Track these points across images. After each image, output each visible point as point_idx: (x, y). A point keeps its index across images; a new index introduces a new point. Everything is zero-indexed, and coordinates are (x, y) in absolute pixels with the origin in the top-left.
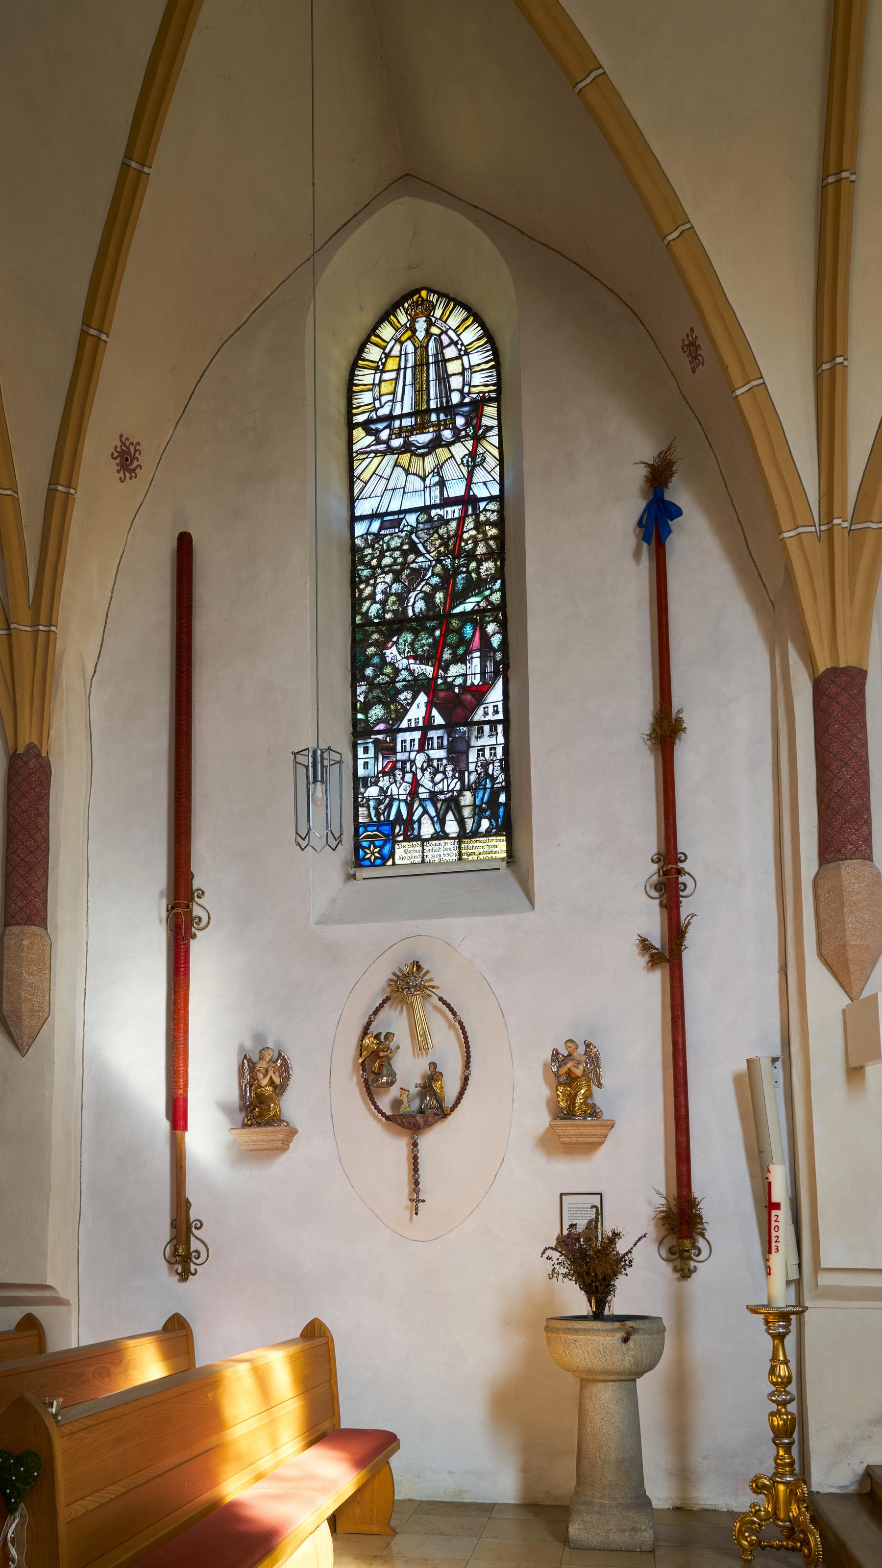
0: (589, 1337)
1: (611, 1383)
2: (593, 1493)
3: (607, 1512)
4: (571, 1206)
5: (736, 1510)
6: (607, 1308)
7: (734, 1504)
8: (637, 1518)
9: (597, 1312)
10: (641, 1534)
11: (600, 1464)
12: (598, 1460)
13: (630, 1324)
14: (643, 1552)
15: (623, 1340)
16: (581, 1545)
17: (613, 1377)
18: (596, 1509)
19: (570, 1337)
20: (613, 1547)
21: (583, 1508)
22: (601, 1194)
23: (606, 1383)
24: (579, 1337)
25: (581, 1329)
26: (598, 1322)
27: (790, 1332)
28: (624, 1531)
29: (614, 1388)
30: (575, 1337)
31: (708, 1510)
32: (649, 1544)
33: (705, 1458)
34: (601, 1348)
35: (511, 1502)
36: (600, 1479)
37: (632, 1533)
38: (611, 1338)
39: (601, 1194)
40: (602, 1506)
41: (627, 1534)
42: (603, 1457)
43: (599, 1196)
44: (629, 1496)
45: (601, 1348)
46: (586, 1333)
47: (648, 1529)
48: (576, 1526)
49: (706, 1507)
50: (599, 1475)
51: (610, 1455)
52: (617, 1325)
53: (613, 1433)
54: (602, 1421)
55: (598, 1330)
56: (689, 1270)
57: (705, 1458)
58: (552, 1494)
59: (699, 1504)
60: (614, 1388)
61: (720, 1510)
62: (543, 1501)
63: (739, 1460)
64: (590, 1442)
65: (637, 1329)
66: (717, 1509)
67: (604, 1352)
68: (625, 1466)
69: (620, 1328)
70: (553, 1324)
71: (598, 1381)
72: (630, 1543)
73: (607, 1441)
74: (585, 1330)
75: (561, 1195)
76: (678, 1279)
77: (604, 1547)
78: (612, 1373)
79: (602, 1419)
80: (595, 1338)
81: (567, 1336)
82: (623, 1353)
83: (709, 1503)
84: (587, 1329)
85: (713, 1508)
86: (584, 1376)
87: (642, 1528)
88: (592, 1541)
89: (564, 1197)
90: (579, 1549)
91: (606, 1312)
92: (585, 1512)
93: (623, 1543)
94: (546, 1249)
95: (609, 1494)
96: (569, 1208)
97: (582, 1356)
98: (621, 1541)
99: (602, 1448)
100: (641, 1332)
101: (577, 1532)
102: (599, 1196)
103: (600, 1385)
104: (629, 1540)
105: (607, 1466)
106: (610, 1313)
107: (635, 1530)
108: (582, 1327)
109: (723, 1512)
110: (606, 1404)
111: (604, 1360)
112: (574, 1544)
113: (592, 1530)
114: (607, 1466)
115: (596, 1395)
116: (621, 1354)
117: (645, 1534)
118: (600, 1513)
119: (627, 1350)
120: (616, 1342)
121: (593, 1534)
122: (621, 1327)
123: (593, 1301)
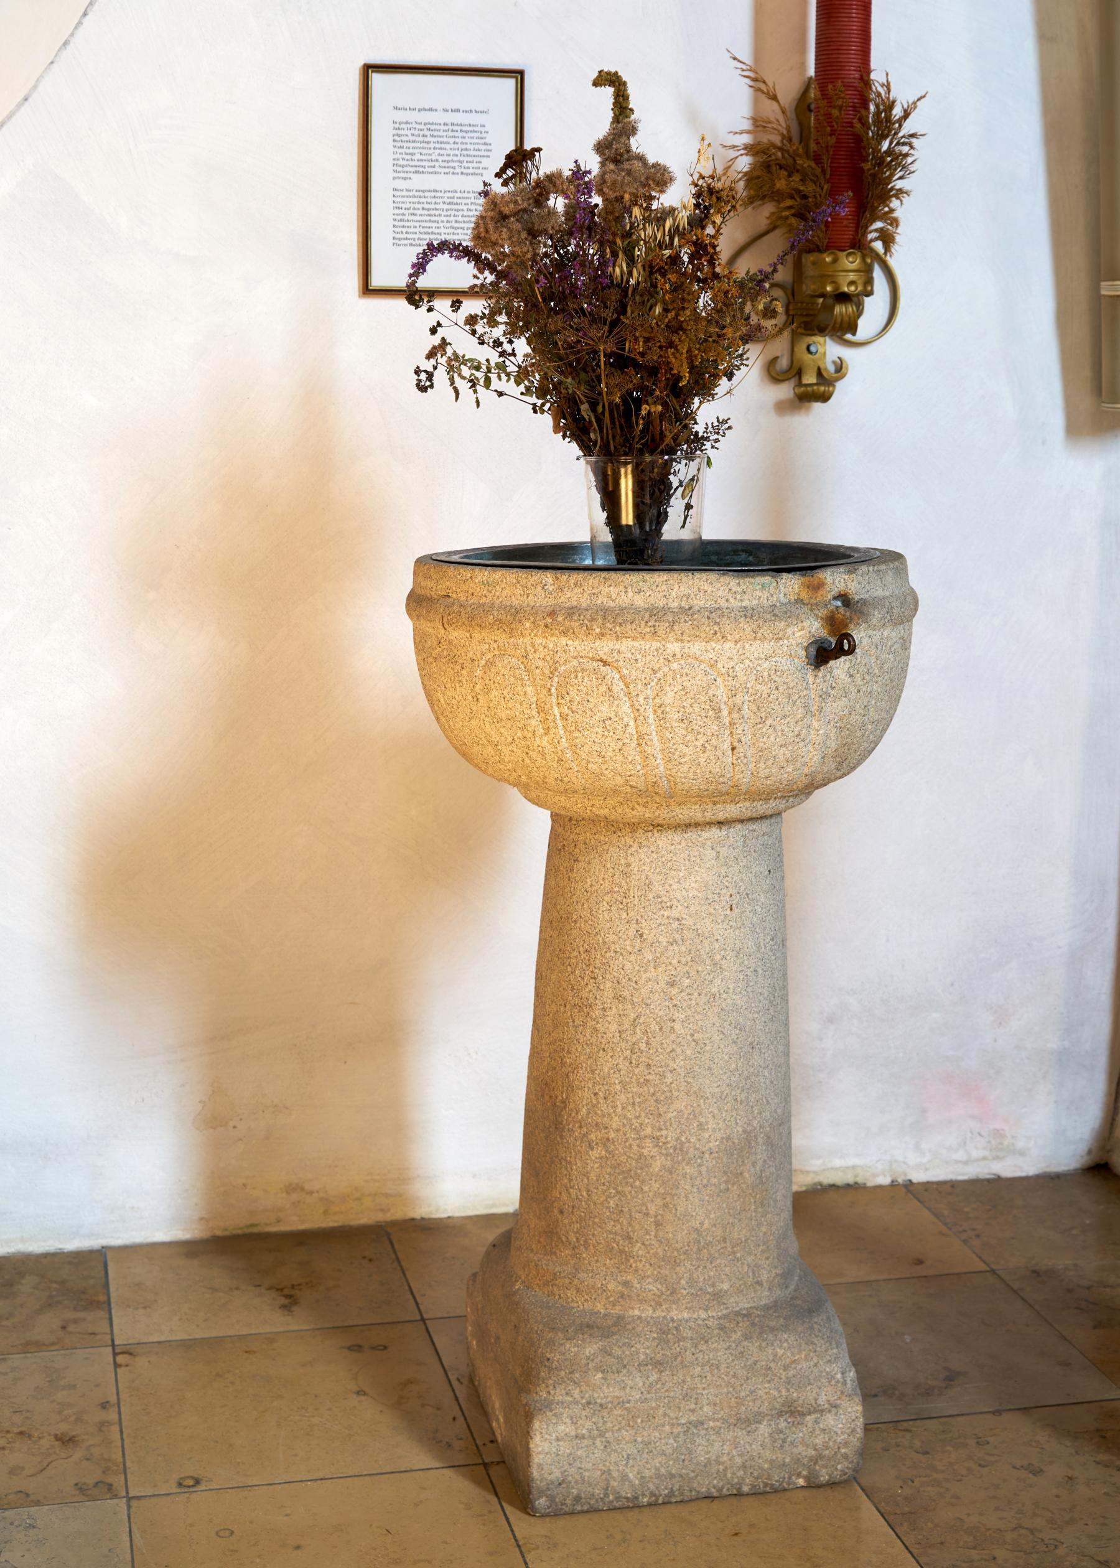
0: (673, 647)
1: (715, 833)
2: (626, 1284)
3: (688, 1357)
4: (401, 116)
5: (918, 1177)
6: (675, 507)
7: (913, 1158)
8: (804, 1365)
9: (637, 531)
10: (816, 1422)
11: (656, 1166)
12: (649, 1149)
13: (835, 580)
14: (819, 1486)
15: (813, 651)
16: (577, 1499)
17: (731, 811)
18: (644, 1348)
19: (577, 645)
20: (704, 1485)
21: (589, 1350)
22: (519, 75)
23: (692, 835)
24: (626, 645)
25: (638, 611)
26: (713, 576)
27: (420, 562)
28: (748, 1422)
29: (724, 851)
30: (604, 647)
31: (833, 1187)
32: (846, 1456)
33: (831, 1020)
34: (721, 691)
35: (161, 1235)
36: (658, 1224)
37: (783, 1425)
38: (768, 647)
39: (519, 75)
40: (666, 1332)
41: (764, 1429)
42: (670, 1135)
43: (510, 84)
44: (764, 1276)
45: (721, 691)
46: (662, 627)
47: (844, 1403)
48: (561, 1428)
49: (827, 1179)
50: (652, 1209)
51: (701, 1126)
52: (790, 585)
53: (716, 1038)
54: (674, 991)
55: (715, 614)
56: (819, 373)
57: (831, 1020)
58: (311, 1193)
59: (808, 1172)
60: (724, 851)
61: (870, 1184)
62: (278, 1221)
63: (935, 1015)
64: (615, 1079)
65: (864, 602)
66: (860, 1180)
67: (736, 709)
68: (754, 1164)
69: (799, 601)
70: (479, 590)
71: (659, 827)
72: (772, 1462)
73: (689, 1072)
74: (654, 613)
75: (369, 69)
76: (783, 408)
77: (672, 1493)
78: (731, 794)
79: (672, 984)
80: (696, 647)
81: (564, 640)
82: (808, 712)
83: (838, 1162)
84: (665, 610)
85: (850, 1179)
86: (576, 806)
87: (822, 1400)
88: (624, 1478)
89: (376, 79)
90: (572, 1513)
91: (671, 531)
92: (598, 1369)
93: (744, 1466)
94: (434, 249)
95: (692, 1282)
96: (398, 126)
97: (631, 729)
98: (739, 1460)
99: (670, 1100)
100: (876, 615)
101: (565, 1448)
102: (510, 84)
103: (664, 841)
104: (768, 1454)
105: (688, 1170)
106: (685, 535)
107: (792, 1411)
108: (639, 601)
109: (881, 1187)
110: (689, 922)
111: (726, 746)
112: (552, 1499)
113: (626, 1434)
114: (688, 1170)
115: (649, 885)
116: (800, 713)
117: (830, 1420)
118: (658, 1365)
119: (824, 697)
120: (784, 663)
121: (631, 1449)
122: (804, 595)
123: (626, 485)
